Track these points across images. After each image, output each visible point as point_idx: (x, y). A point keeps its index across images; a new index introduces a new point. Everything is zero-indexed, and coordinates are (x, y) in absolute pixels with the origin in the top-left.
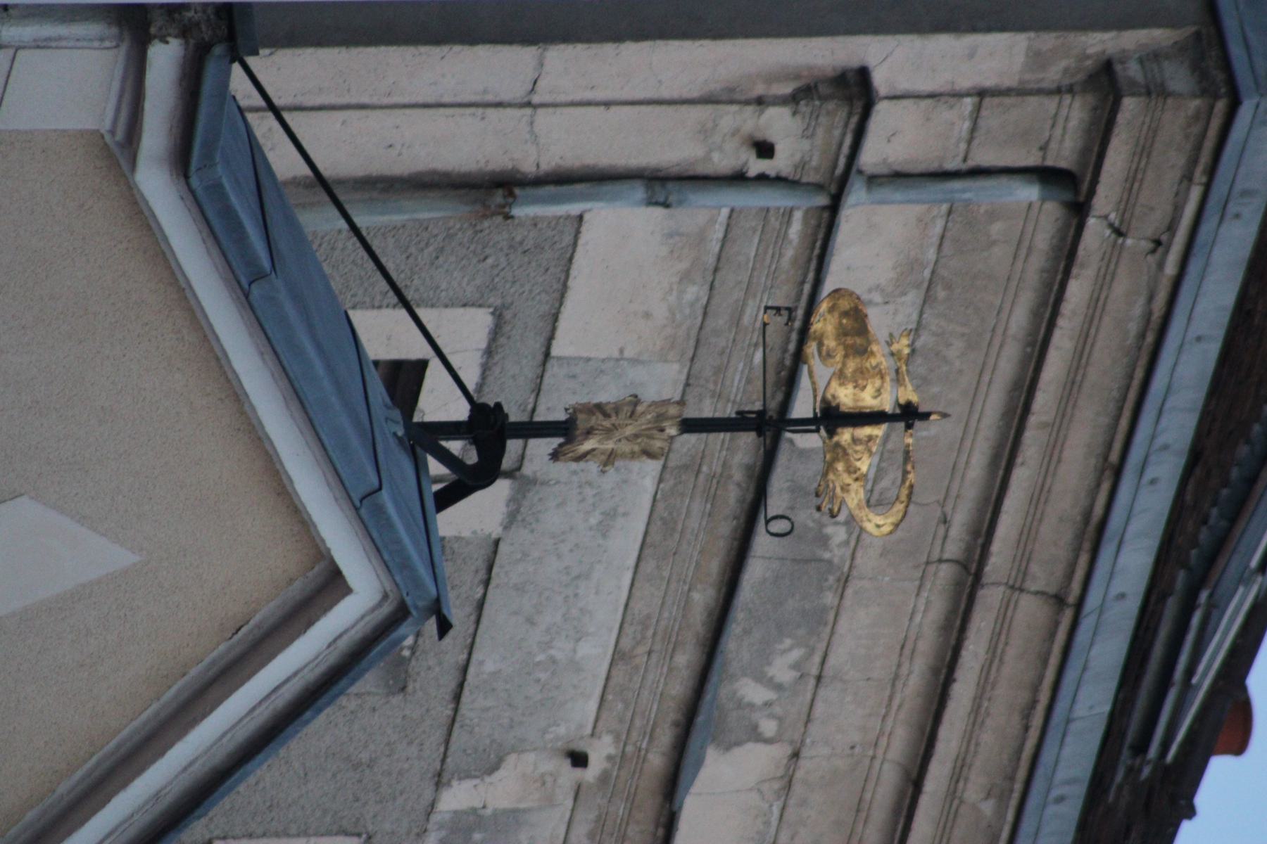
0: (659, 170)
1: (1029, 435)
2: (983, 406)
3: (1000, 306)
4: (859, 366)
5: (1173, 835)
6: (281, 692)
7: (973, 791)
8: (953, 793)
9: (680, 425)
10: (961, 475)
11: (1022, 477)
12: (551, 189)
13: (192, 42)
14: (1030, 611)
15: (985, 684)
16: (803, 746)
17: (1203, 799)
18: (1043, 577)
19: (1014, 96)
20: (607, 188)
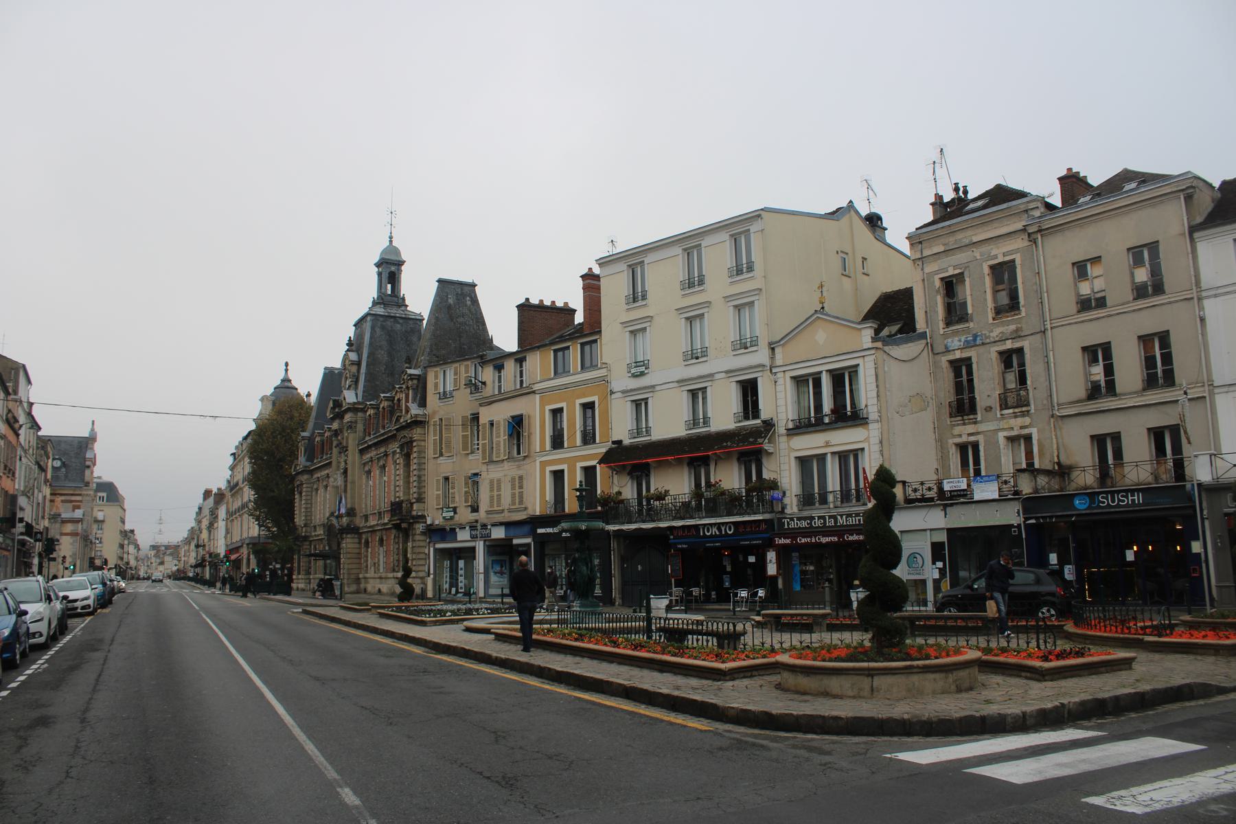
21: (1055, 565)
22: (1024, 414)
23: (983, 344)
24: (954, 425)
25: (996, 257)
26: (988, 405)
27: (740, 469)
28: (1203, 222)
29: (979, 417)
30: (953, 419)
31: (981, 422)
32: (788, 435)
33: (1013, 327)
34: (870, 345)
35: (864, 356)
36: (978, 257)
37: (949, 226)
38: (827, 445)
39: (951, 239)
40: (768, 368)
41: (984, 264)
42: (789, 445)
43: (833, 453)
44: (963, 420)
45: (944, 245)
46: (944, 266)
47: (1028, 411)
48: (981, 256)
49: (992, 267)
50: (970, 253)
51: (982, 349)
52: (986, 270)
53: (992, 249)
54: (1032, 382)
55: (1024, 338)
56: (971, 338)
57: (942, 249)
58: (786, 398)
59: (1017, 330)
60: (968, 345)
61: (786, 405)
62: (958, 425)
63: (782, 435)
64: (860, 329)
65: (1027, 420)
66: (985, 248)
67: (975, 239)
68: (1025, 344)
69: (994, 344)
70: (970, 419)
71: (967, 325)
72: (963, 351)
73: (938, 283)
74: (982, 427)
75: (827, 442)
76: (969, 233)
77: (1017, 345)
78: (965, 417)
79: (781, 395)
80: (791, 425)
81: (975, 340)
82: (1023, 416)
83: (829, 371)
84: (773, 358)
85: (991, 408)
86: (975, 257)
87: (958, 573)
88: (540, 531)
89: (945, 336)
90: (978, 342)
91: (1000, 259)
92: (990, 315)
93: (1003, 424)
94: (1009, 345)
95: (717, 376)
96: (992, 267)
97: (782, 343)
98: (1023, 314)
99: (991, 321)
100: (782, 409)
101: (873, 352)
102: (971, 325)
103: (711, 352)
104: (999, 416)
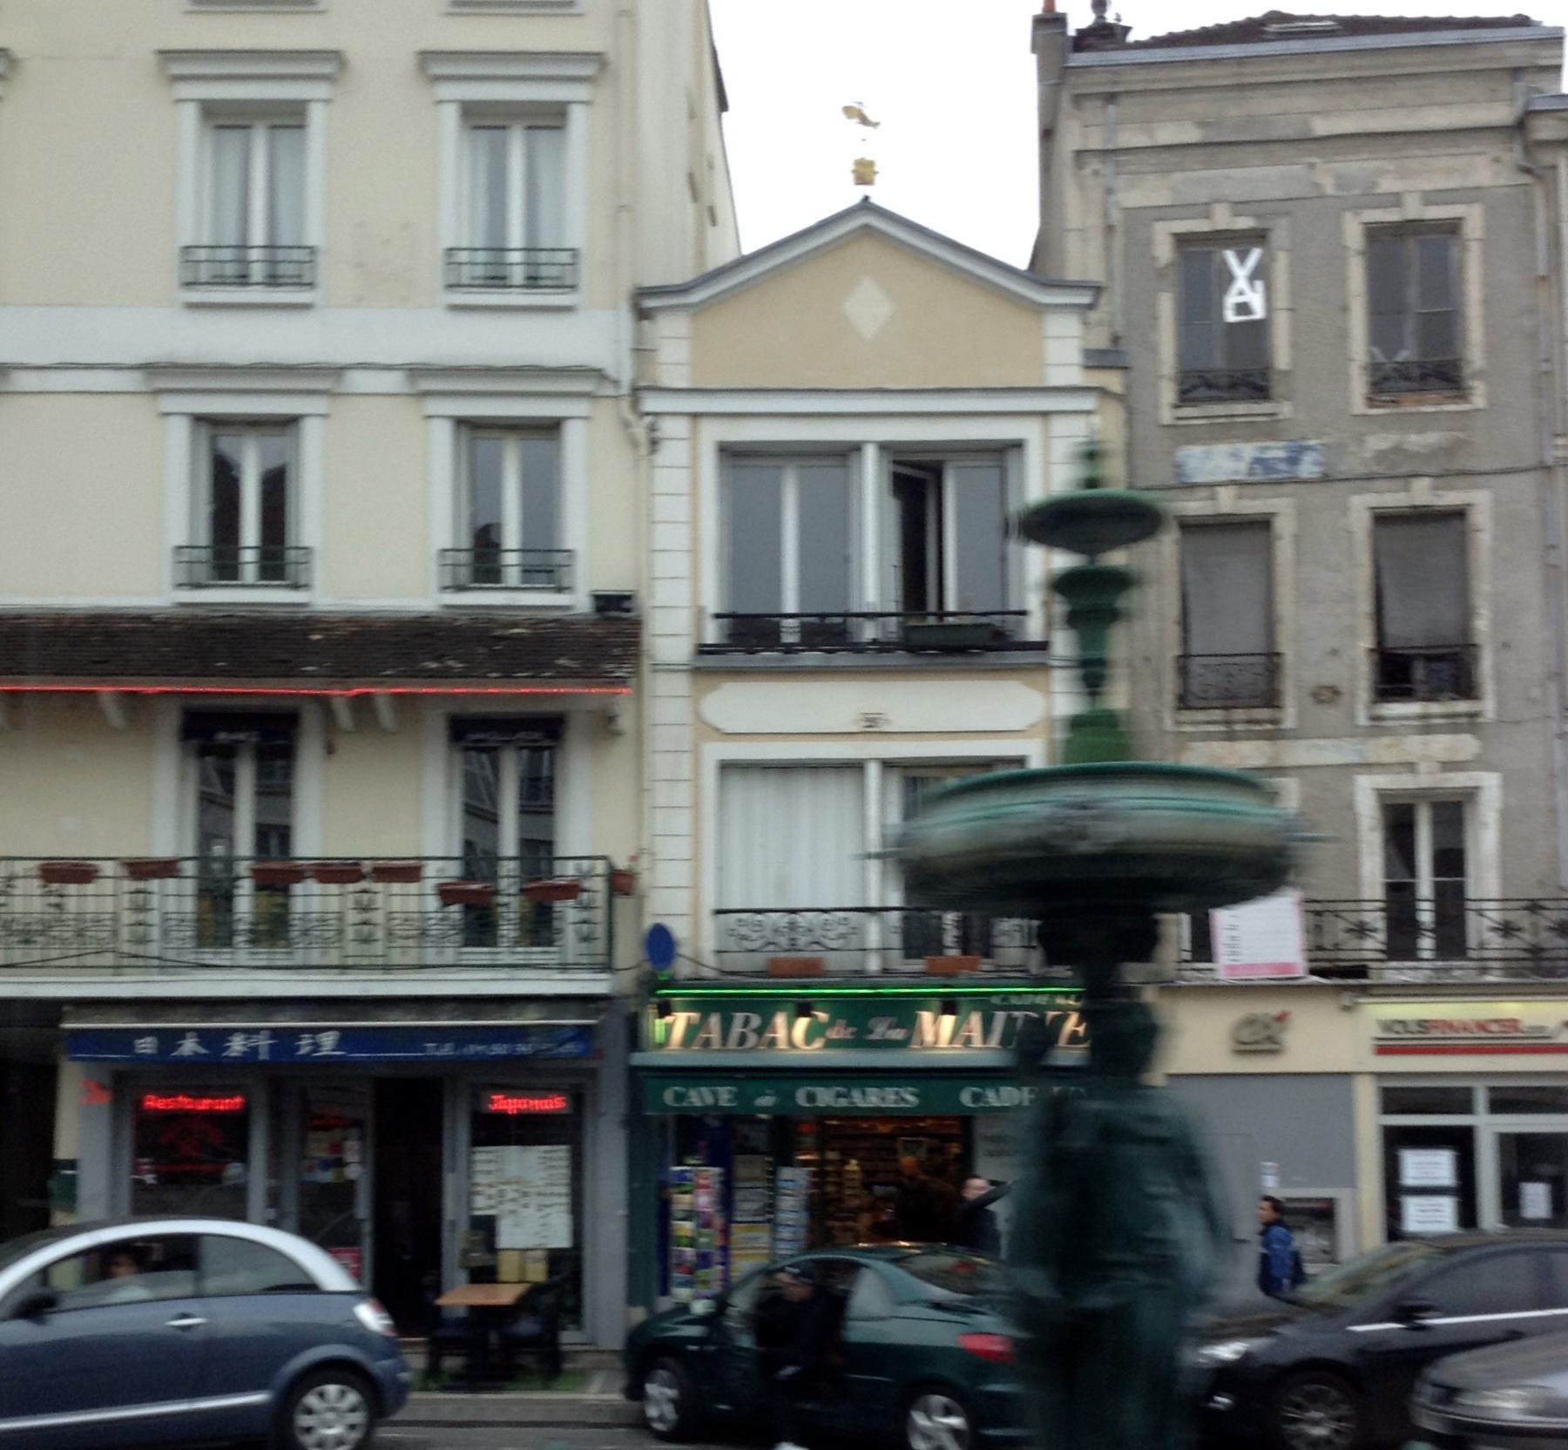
0: (429, 365)
1: (1088, 92)
2: (1259, 415)
3: (621, 396)
4: (655, 1006)
5: (774, 1447)
6: (264, 963)
7: (1313, 66)
8: (1314, 71)
9: (1299, 904)
10: (1146, 492)
11: (1206, 83)
12: (277, 371)
13: (599, 631)
14: (1248, 70)
15: (1272, 73)
16: (811, 970)
17: (1032, 61)
18: (1236, 69)
19: (1372, 356)
20: (197, 287)
21: (1445, 1178)
22: (1454, 725)
23: (1326, 479)
24: (1193, 737)
25: (1396, 200)
26: (1327, 680)
27: (183, 778)
28: (1119, 395)
29: (1289, 718)
30: (1187, 715)
31: (1294, 735)
32: (696, 672)
33: (1433, 438)
34: (1075, 377)
35: (1045, 414)
36: (1330, 190)
37: (1240, 61)
38: (872, 728)
39: (1234, 110)
40: (625, 390)
41: (1348, 216)
42: (698, 715)
43: (888, 765)
44: (1228, 723)
45: (1202, 124)
46: (1202, 195)
47: (1472, 715)
48: (1339, 186)
49: (1374, 233)
50: (1298, 169)
51: (1320, 495)
52: (1353, 234)
53: (1382, 172)
54: (1496, 623)
55: (1479, 479)
56: (1281, 454)
57: (1192, 134)
58: (694, 521)
59: (1450, 450)
60: (1266, 477)
61: (694, 551)
62: (1208, 737)
63: (671, 669)
64: (1040, 309)
65: (1466, 745)
66: (1358, 166)
67: (1321, 127)
68: (1480, 501)
69: (1365, 484)
70: (1258, 722)
71: (1265, 407)
72: (1247, 490)
73: (1164, 251)
74: (1299, 753)
75: (872, 721)
76: (1301, 101)
77: (1450, 498)
78: (1240, 714)
79: (671, 509)
80: (712, 634)
81: (1293, 461)
82: (1454, 729)
83: (884, 447)
84: (642, 352)
85: (1335, 692)
86: (1317, 185)
87: (263, 1062)
88: (154, 1102)
89: (1182, 434)
90: (1308, 467)
91: (1413, 209)
92: (1359, 385)
93: (1378, 749)
94: (1422, 494)
95: (360, 381)
96: (1374, 233)
97: (696, 297)
98: (1479, 400)
99: (1358, 405)
100: (671, 565)
101: (1087, 403)
102: (1285, 410)
103: (333, 275)
104: (1362, 720)
